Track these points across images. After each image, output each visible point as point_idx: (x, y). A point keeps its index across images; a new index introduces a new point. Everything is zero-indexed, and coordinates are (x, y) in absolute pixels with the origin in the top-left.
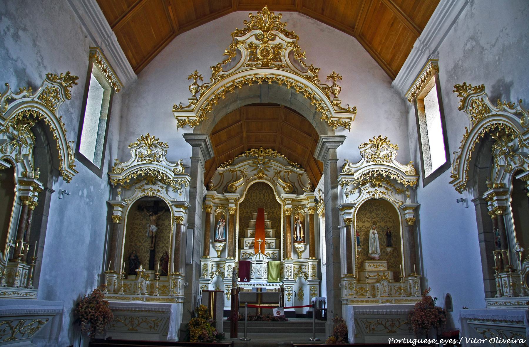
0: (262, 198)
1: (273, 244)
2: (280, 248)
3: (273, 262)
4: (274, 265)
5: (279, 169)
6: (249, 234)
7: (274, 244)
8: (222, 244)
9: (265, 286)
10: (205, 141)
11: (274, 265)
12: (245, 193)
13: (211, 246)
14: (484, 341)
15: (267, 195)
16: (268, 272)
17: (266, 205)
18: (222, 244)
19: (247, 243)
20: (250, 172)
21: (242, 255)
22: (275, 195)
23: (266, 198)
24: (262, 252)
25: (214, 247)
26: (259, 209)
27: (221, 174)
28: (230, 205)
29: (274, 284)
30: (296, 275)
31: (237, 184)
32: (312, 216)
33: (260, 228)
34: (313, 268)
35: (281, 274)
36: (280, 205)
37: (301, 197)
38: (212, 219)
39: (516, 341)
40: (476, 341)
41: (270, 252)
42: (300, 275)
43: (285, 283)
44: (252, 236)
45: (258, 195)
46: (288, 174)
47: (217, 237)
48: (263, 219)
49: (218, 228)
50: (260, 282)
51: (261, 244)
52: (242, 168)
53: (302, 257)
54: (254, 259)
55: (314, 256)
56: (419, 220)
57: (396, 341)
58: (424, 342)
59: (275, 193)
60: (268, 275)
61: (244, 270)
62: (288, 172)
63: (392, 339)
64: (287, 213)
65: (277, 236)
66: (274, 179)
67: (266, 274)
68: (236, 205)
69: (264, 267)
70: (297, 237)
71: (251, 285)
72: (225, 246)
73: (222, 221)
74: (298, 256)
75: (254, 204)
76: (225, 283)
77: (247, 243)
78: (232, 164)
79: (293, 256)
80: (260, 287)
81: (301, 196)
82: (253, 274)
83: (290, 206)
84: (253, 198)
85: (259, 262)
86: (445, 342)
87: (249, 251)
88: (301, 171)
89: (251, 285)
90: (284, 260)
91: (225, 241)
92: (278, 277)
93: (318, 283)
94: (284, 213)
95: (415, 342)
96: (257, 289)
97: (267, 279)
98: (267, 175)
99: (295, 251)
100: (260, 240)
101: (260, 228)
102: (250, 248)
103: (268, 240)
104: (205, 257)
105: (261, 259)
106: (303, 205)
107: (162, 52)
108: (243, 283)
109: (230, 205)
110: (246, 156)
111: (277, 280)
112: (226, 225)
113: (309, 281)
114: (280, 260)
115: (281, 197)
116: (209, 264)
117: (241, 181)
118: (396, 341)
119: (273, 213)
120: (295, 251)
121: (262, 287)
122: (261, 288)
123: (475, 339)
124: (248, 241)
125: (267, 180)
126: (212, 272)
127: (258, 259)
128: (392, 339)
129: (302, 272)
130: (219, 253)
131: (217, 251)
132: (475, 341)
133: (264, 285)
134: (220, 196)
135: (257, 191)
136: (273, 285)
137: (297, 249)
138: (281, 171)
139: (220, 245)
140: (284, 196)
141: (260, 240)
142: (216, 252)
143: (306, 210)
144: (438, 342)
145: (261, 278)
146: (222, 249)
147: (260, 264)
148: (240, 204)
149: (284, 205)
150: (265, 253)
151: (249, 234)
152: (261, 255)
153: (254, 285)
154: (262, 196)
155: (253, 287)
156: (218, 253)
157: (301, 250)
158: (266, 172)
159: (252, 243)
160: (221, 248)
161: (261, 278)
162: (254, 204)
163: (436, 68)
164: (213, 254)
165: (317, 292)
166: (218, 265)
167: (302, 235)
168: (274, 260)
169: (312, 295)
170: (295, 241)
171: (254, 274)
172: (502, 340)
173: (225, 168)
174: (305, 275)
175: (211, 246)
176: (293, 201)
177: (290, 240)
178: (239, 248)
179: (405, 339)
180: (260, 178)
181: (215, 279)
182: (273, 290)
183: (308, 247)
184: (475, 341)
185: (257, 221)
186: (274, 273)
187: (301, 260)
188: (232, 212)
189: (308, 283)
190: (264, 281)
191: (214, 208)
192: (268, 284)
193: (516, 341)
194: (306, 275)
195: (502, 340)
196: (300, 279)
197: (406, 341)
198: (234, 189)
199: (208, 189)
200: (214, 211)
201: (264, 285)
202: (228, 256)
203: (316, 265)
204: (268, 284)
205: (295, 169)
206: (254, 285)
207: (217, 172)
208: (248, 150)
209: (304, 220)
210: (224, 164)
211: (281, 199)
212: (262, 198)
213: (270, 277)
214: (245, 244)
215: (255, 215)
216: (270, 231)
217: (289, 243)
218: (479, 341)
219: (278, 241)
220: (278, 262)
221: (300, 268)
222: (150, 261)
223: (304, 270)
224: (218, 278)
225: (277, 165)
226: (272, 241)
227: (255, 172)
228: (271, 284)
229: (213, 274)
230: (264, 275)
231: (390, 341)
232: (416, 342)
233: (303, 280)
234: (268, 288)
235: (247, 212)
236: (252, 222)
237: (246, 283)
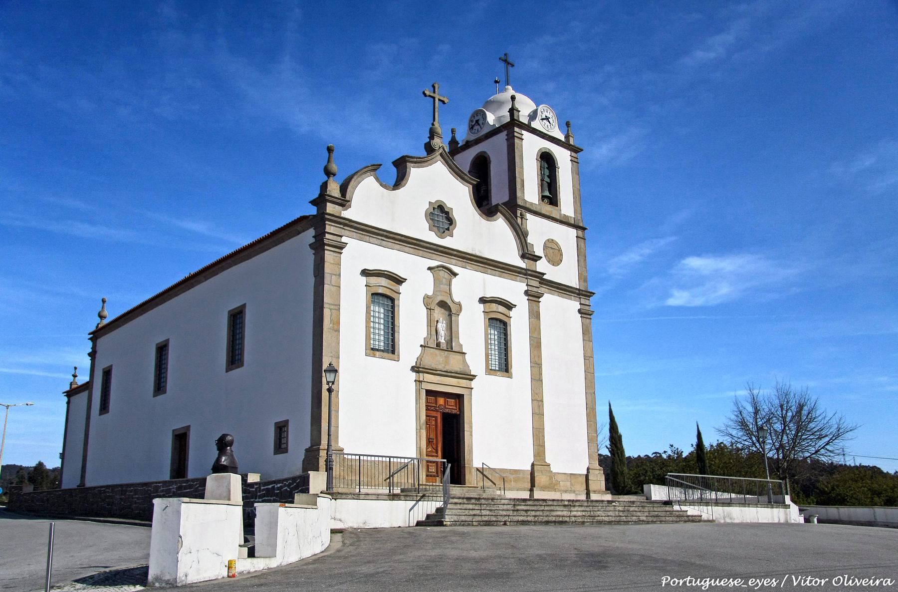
10: (436, 418)
14: (823, 582)
39: (877, 582)
40: (811, 581)
56: (620, 437)
58: (722, 583)
63: (667, 579)
76: (451, 501)
86: (757, 585)
107: (478, 254)
123: (809, 578)
128: (667, 579)
144: (746, 583)
163: (538, 377)
179: (689, 578)
182: (337, 442)
193: (877, 582)
197: (691, 582)
218: (816, 582)
222: (322, 308)
231: (664, 582)
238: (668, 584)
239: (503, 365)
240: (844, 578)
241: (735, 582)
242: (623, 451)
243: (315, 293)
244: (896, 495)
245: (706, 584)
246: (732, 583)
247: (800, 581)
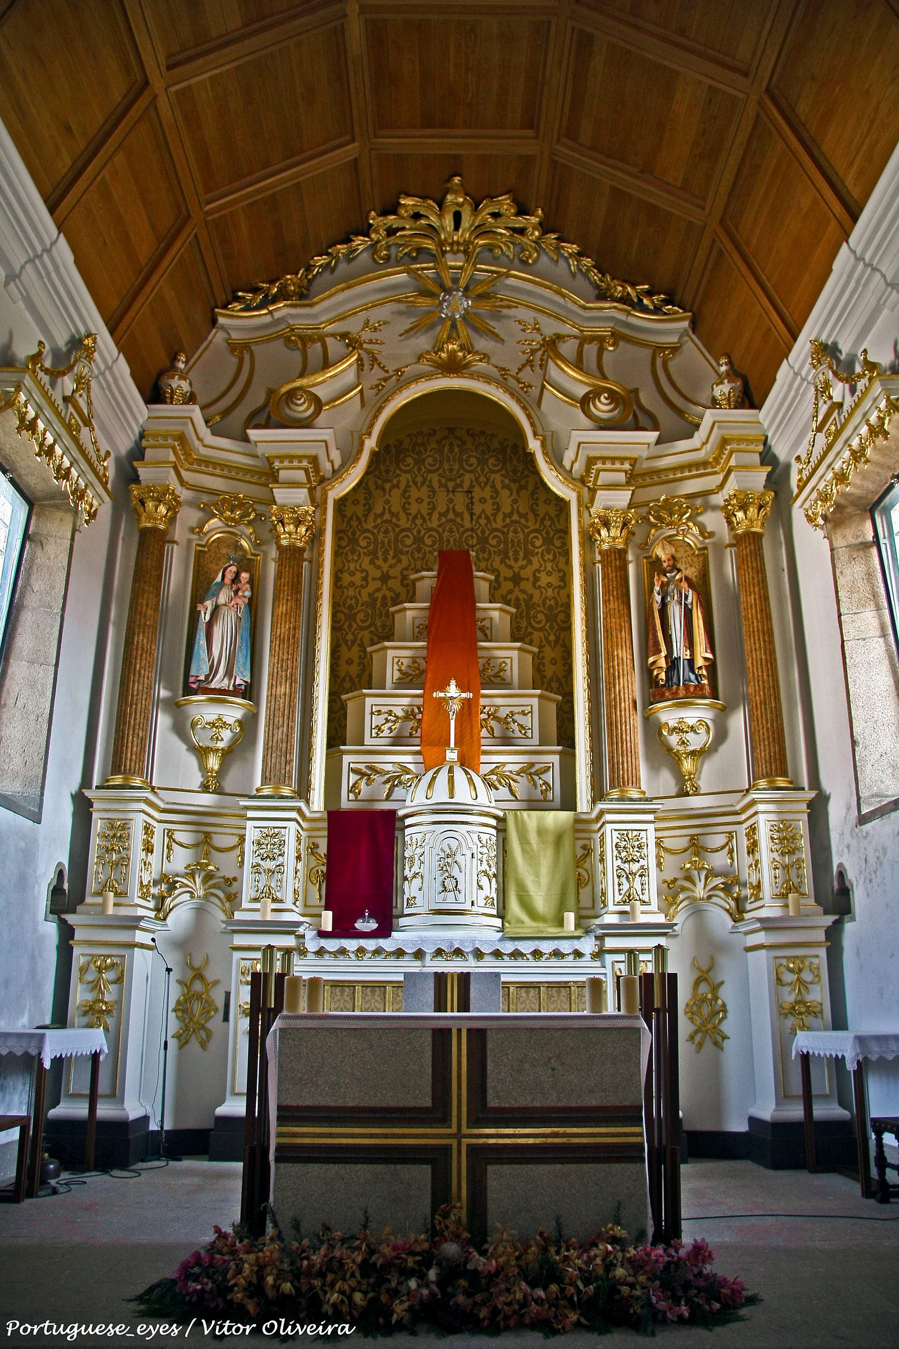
0: (460, 508)
1: (526, 721)
2: (567, 739)
3: (532, 819)
4: (541, 832)
5: (551, 327)
6: (392, 674)
7: (532, 722)
8: (233, 712)
9: (489, 965)
11: (541, 832)
12: (371, 444)
13: (163, 721)
15: (487, 492)
16: (504, 874)
17: (483, 541)
18: (233, 712)
19: (378, 720)
20: (400, 347)
21: (348, 779)
22: (530, 458)
23: (478, 509)
24: (467, 762)
25: (180, 729)
26: (444, 556)
27: (239, 349)
28: (281, 495)
29: (546, 947)
30: (671, 892)
31: (324, 384)
32: (749, 545)
33: (452, 636)
34: (785, 840)
35: (579, 885)
36: (562, 505)
37: (683, 450)
38: (177, 574)
39: (330, 1329)
41: (511, 761)
42: (700, 891)
43: (610, 943)
44: (407, 680)
45: (442, 499)
46: (601, 351)
47: (200, 669)
48: (470, 599)
49: (205, 617)
50: (456, 937)
51: (460, 716)
52: (353, 326)
53: (704, 784)
54: (413, 800)
55: (784, 773)
57: (25, 1330)
58: (97, 1330)
59: (534, 445)
60: (503, 892)
61: (361, 867)
62: (601, 340)
64: (608, 538)
65: (554, 679)
66: (527, 375)
67: (490, 889)
68: (319, 503)
69: (475, 842)
70: (673, 664)
71: (399, 953)
72: (248, 725)
73: (236, 579)
74: (680, 777)
75: (419, 540)
77: (378, 720)
78: (303, 295)
79: (650, 780)
80: (454, 967)
81: (683, 445)
82: (411, 889)
83: (623, 498)
84: (414, 509)
85: (449, 812)
87: (389, 762)
88: (673, 328)
89: (399, 953)
90: (598, 795)
91: (249, 692)
92: (561, 908)
93: (821, 936)
94: (588, 540)
95: (73, 1332)
96: (440, 979)
97: (501, 915)
98: (486, 357)
99: (663, 754)
100: (453, 690)
101: (452, 636)
102: (398, 740)
103: (494, 699)
104: (118, 780)
105: (463, 794)
106: (691, 496)
108: (351, 944)
109: (281, 495)
110: (374, 248)
111: (560, 922)
112: (254, 606)
113: (768, 925)
114: (568, 802)
115: (568, 457)
116: (138, 822)
117: (344, 370)
118: (25, 1330)
119: (516, 579)
120: (663, 754)
121: (469, 965)
122: (465, 979)
123: (227, 1324)
124: (383, 707)
125: (488, 379)
126: (164, 878)
127: (440, 794)
129: (711, 873)
130: (213, 762)
131: (202, 753)
132: (225, 1329)
133: (478, 954)
134: (225, 448)
135: (435, 478)
136: (537, 954)
137: (674, 740)
138: (559, 337)
139: (220, 716)
140: (583, 439)
141: (453, 690)
142: (192, 761)
143: (713, 521)
145: (467, 902)
146: (234, 742)
147: (456, 835)
148: (341, 504)
149: (585, 506)
150: (484, 769)
151: (392, 674)
152: (459, 774)
153: (419, 954)
154: (460, 502)
155: (415, 967)
156: (203, 768)
157: (696, 741)
158: (482, 344)
159: (409, 715)
160: (226, 735)
161: (467, 902)
162: (419, 540)
164: (174, 767)
165: (819, 994)
166: (204, 832)
167: (702, 653)
168: (534, 805)
169: (794, 1013)
170: (656, 690)
171: (417, 888)
172: (294, 1327)
173: (261, 317)
174: (727, 889)
175: (163, 721)
176: (638, 476)
177: (632, 686)
178: (335, 739)
179: (47, 1323)
180: (453, 367)
181: (181, 915)
183: (738, 722)
184: (225, 1329)
185: (433, 609)
186: (539, 882)
187: (695, 802)
188: (291, 535)
189: (761, 938)
190: (483, 930)
191: (188, 516)
192: (508, 947)
193: (330, 1329)
194: (736, 893)
195: (294, 1327)
196: (697, 911)
197: (50, 1328)
198: (303, 409)
199: (154, 395)
200: (191, 530)
201: (478, 954)
202: (265, 780)
203: (802, 826)
204: (508, 947)
205: (639, 319)
206: (419, 954)
207: (217, 337)
208: (384, 213)
209: (704, 575)
210: (255, 290)
211: (567, 475)
212: (460, 508)
213: (514, 906)
214: (371, 721)
215: (427, 580)
216: (510, 656)
217: (626, 705)
218: (238, 1330)
219: (552, 708)
220: (565, 816)
221: (696, 847)
223: (720, 860)
224: (200, 912)
225: (547, 297)
226: (526, 707)
227: (423, 342)
228: (526, 947)
229: (172, 887)
230: (476, 890)
231: (10, 1329)
232: (76, 1330)
233: (719, 917)
234: (512, 972)
235: (385, 578)
236: (412, 613)
237: (370, 944)
238: (16, 1332)
239: (797, 1087)
240: (279, 1323)
241: (117, 1329)
242: (427, 1108)
243: (329, 707)
244: (873, 1018)
245: (73, 1332)
246: (113, 1330)
247: (214, 1328)
